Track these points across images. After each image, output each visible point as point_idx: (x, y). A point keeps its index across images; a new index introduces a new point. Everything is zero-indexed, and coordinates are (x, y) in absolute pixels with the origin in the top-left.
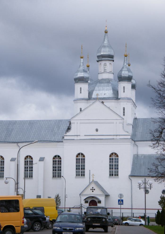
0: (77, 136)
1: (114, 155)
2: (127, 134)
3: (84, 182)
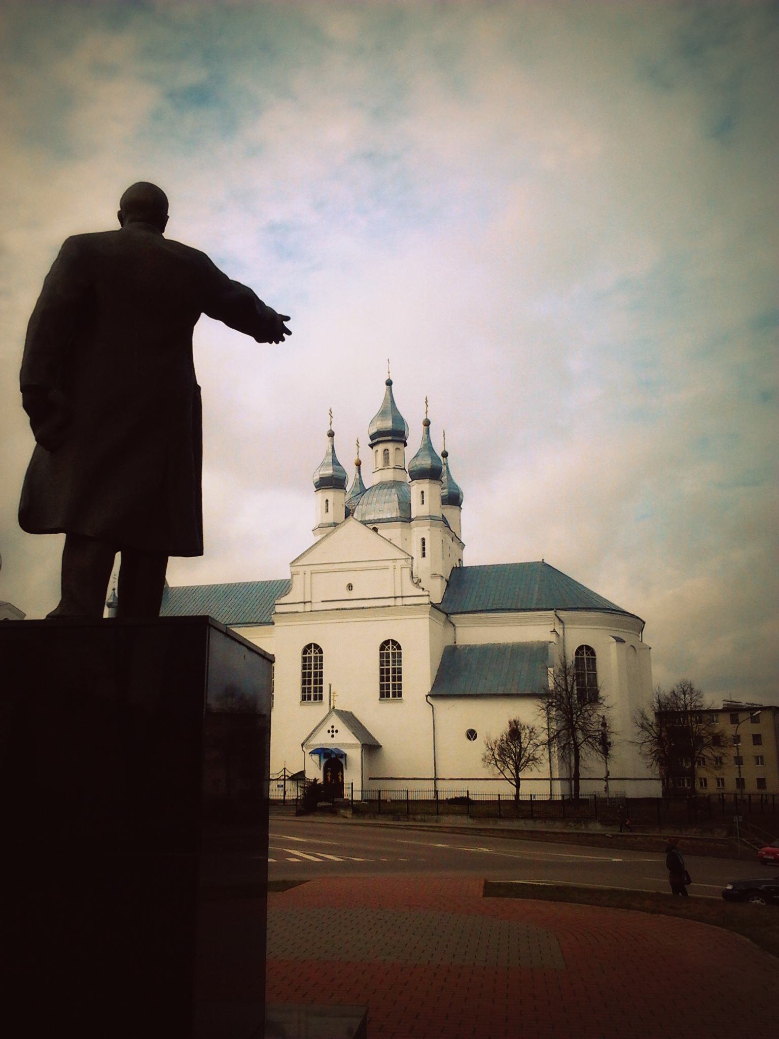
2: (420, 592)
3: (317, 711)
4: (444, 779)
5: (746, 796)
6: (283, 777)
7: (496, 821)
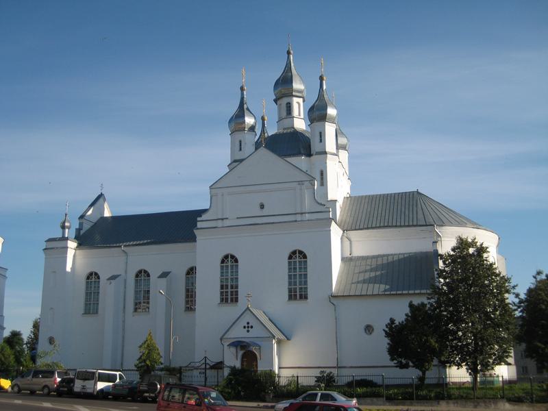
0: (222, 219)
1: (297, 255)
3: (231, 311)
4: (345, 367)
5: (196, 373)
7: (478, 403)
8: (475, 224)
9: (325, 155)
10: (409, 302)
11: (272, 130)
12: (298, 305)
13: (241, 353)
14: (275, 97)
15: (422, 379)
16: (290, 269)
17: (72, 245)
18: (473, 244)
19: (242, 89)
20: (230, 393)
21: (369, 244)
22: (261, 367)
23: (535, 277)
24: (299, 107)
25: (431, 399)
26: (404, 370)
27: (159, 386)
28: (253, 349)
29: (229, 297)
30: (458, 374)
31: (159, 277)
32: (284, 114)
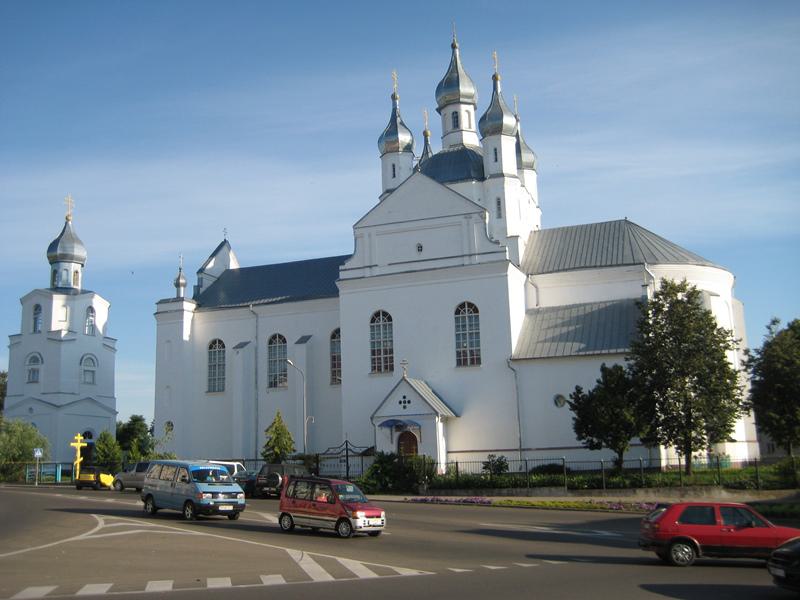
3: (385, 382)
6: (345, 453)
7: (686, 491)
8: (702, 259)
9: (501, 179)
10: (600, 364)
11: (436, 148)
12: (469, 372)
13: (396, 435)
14: (437, 106)
15: (618, 462)
16: (457, 327)
17: (189, 307)
18: (682, 288)
19: (394, 97)
20: (374, 485)
21: (565, 291)
22: (422, 451)
23: (769, 328)
24: (468, 117)
25: (625, 487)
26: (597, 451)
27: (280, 479)
28: (410, 429)
29: (383, 365)
30: (669, 456)
31: (296, 343)
32: (450, 127)
